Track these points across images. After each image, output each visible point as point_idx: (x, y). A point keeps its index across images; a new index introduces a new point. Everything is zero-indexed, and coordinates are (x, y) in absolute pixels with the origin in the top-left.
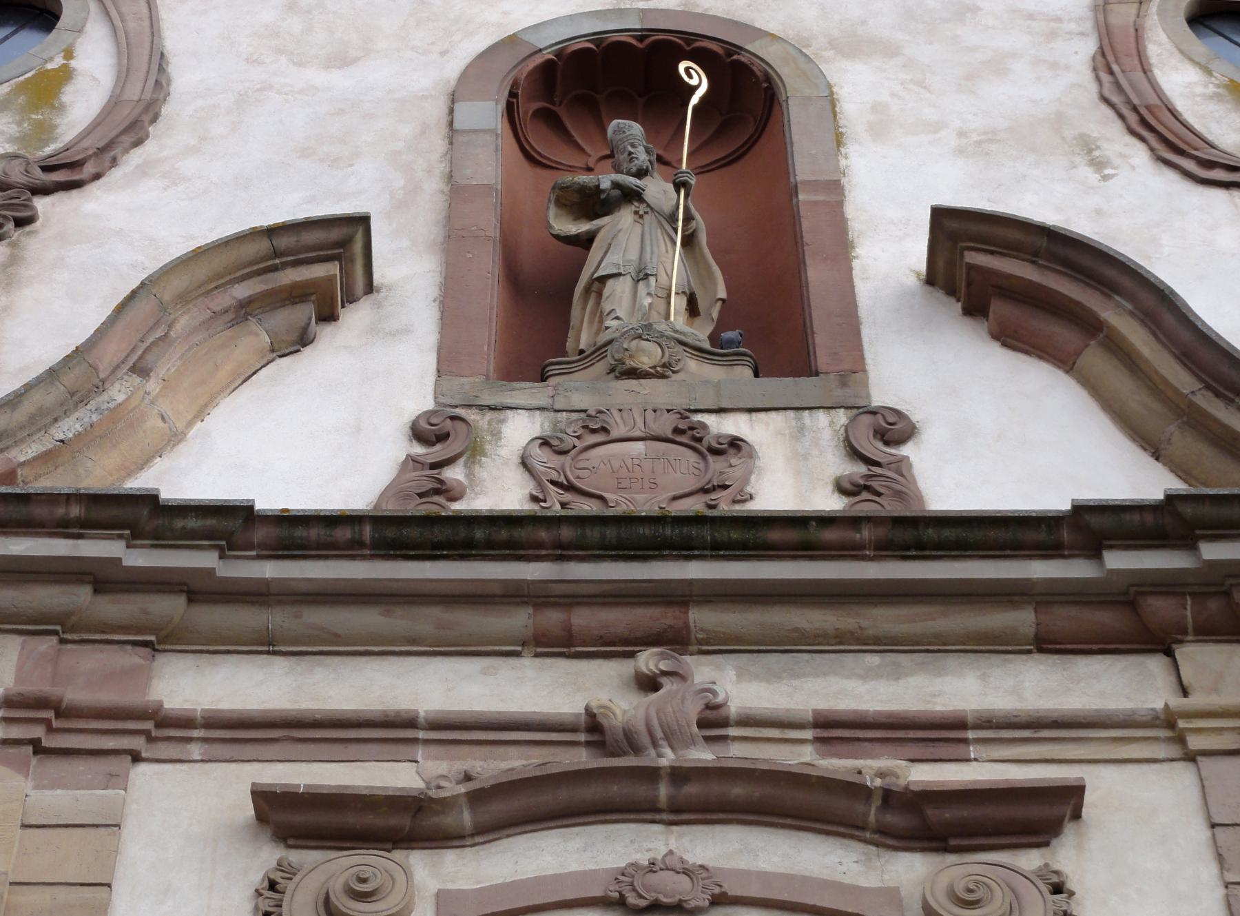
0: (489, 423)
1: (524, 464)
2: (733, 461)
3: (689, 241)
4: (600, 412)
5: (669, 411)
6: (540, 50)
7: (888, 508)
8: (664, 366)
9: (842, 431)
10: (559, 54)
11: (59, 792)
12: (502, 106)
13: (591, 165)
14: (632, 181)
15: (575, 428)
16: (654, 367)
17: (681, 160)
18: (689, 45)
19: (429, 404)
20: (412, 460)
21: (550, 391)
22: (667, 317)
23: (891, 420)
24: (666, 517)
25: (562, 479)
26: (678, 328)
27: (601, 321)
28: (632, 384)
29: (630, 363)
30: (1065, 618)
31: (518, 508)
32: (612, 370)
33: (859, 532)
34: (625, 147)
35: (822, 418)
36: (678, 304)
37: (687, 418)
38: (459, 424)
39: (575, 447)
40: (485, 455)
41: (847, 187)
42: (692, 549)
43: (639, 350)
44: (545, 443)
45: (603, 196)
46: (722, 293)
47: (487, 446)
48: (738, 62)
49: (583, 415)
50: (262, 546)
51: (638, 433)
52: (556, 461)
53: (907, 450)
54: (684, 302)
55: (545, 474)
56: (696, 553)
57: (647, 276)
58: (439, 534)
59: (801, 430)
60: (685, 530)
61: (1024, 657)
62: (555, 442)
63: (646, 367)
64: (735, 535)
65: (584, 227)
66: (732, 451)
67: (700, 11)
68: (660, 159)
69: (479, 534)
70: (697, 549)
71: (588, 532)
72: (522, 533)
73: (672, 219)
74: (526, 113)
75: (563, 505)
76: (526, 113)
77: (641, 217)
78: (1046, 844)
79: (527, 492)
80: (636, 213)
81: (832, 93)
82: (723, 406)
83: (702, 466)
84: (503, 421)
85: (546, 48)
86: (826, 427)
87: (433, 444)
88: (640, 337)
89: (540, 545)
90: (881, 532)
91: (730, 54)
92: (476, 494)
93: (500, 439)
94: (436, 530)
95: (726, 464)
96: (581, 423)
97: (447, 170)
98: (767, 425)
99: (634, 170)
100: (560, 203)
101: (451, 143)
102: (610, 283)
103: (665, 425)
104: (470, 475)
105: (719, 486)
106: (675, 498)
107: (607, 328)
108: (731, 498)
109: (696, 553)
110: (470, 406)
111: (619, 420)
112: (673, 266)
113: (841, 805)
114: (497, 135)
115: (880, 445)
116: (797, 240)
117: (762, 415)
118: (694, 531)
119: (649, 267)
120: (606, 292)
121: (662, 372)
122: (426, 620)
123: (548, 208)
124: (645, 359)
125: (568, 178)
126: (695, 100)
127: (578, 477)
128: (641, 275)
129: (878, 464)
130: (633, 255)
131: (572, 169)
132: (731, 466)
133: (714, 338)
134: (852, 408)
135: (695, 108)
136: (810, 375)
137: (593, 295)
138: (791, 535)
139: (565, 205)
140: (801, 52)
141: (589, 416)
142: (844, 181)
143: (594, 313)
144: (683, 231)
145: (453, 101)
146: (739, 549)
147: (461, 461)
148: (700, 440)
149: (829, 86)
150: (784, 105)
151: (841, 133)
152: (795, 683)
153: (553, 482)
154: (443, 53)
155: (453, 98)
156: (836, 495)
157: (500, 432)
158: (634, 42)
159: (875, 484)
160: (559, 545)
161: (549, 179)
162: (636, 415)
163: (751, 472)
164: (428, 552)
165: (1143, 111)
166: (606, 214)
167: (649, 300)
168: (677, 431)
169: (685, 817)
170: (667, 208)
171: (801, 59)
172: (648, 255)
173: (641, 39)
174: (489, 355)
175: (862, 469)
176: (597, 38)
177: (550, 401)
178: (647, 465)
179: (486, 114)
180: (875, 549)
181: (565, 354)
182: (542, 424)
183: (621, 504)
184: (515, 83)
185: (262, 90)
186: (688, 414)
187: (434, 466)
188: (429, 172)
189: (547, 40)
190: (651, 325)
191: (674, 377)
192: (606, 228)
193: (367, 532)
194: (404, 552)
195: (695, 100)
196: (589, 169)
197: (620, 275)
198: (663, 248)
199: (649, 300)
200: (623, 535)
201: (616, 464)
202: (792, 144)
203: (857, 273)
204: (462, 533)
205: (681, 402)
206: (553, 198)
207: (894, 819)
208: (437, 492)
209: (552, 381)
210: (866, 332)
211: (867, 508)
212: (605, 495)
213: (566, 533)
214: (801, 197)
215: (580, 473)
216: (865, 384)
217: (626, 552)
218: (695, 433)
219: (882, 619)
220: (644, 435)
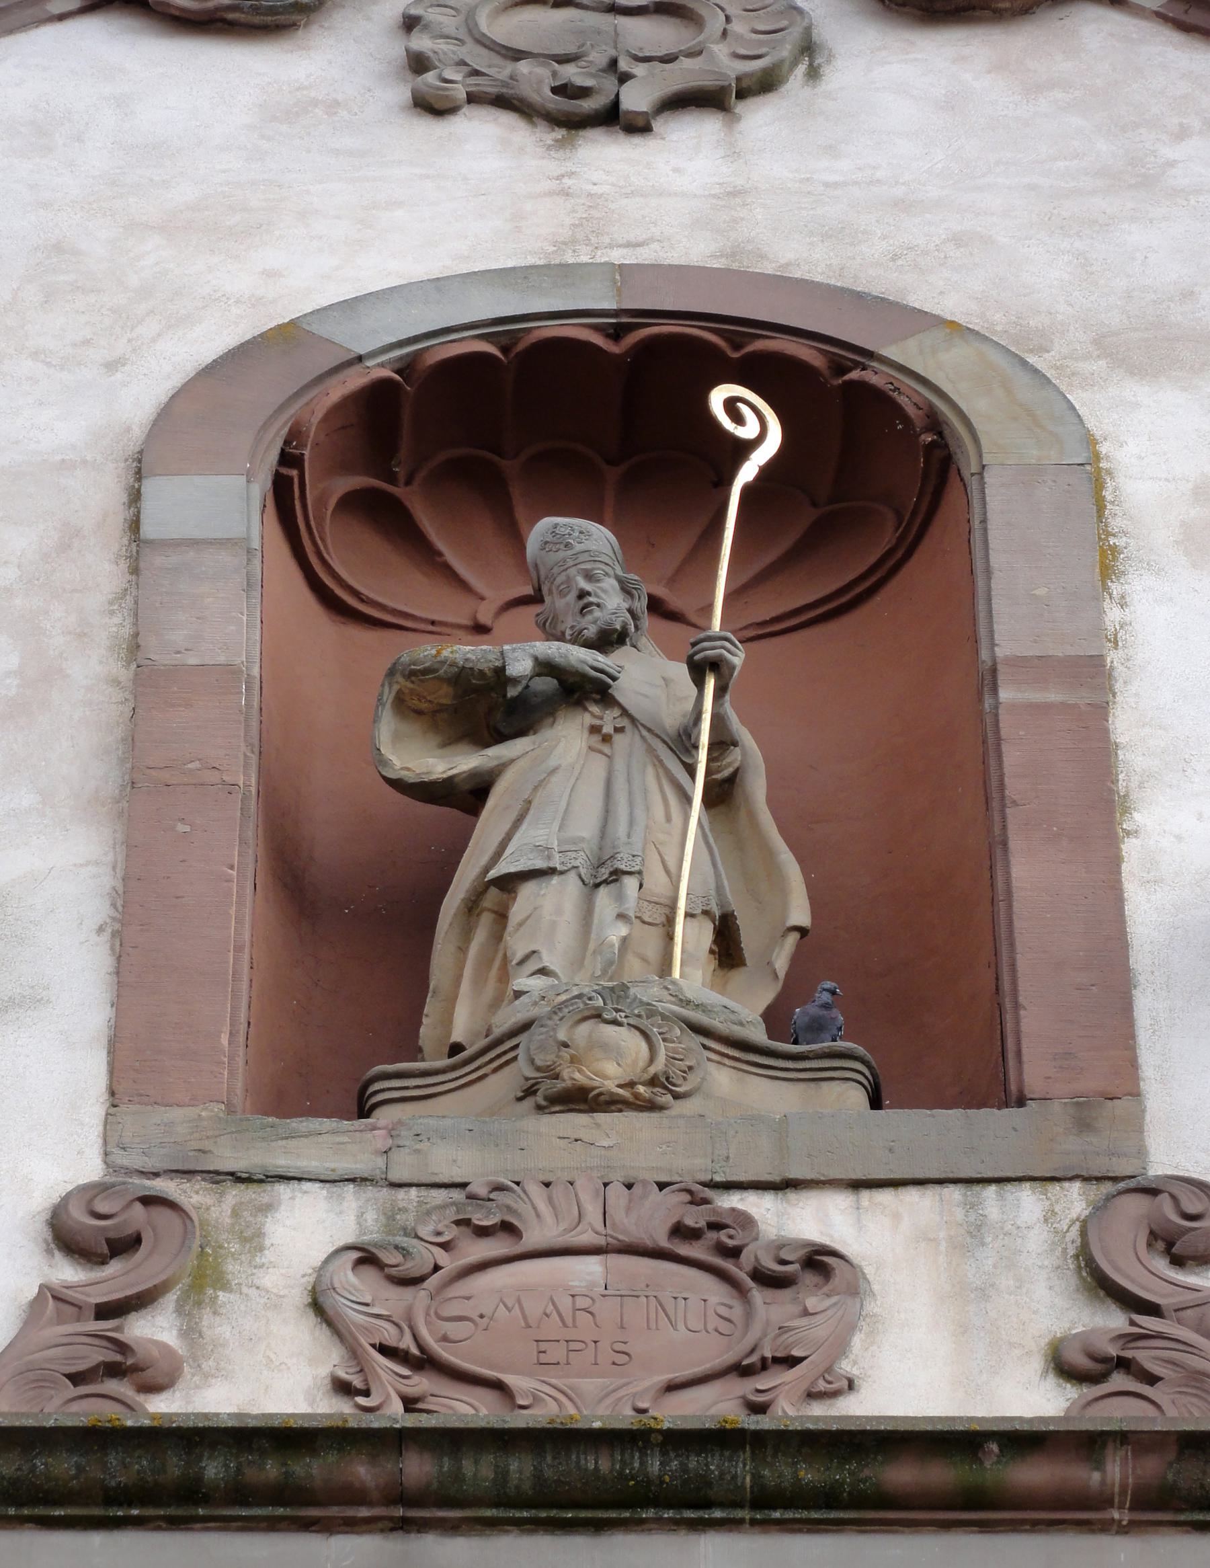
0: (235, 1213)
1: (318, 1307)
2: (812, 1303)
3: (722, 794)
4: (499, 1188)
5: (662, 1186)
6: (360, 359)
7: (1171, 1412)
8: (653, 1082)
9: (1075, 1231)
10: (407, 368)
12: (262, 485)
13: (485, 618)
14: (579, 657)
15: (438, 1225)
16: (631, 1085)
17: (710, 607)
18: (737, 347)
19: (91, 1169)
20: (54, 1298)
21: (380, 1140)
22: (665, 968)
23: (1192, 1208)
24: (651, 1431)
25: (407, 1343)
26: (689, 995)
27: (504, 976)
28: (577, 1123)
29: (573, 1076)
31: (303, 1408)
32: (530, 1092)
33: (1099, 1466)
34: (569, 580)
36: (691, 937)
37: (706, 1201)
38: (161, 1215)
39: (437, 1268)
40: (225, 1286)
41: (1120, 671)
42: (708, 1505)
43: (595, 1045)
44: (367, 1258)
45: (512, 692)
46: (800, 915)
47: (231, 1267)
48: (862, 385)
49: (457, 1195)
51: (586, 1237)
52: (393, 1300)
54: (705, 934)
55: (366, 1330)
56: (718, 1514)
57: (617, 875)
58: (120, 1469)
59: (976, 1231)
60: (693, 1462)
62: (389, 1258)
63: (611, 1086)
64: (808, 1474)
65: (463, 762)
66: (809, 1278)
67: (769, 268)
68: (656, 606)
69: (213, 1469)
70: (722, 1505)
71: (468, 1467)
72: (313, 1469)
73: (684, 743)
74: (321, 501)
75: (410, 1404)
76: (321, 501)
77: (607, 739)
79: (324, 1371)
80: (595, 730)
81: (1097, 457)
82: (795, 1173)
83: (737, 1312)
84: (267, 1208)
85: (373, 354)
86: (1034, 1223)
87: (103, 1261)
88: (598, 1016)
89: (355, 1496)
90: (1151, 1468)
91: (840, 368)
92: (206, 1376)
93: (261, 1249)
94: (113, 1460)
95: (797, 1309)
96: (451, 1214)
97: (127, 631)
98: (896, 1217)
99: (591, 632)
100: (402, 705)
101: (135, 570)
102: (527, 891)
103: (653, 1218)
104: (190, 1333)
105: (776, 1360)
106: (672, 1387)
107: (518, 994)
108: (804, 1386)
109: (718, 1514)
110: (188, 1173)
111: (543, 1207)
112: (683, 852)
114: (249, 551)
115: (1161, 1265)
116: (989, 794)
117: (885, 1197)
118: (714, 1464)
119: (622, 855)
120: (518, 911)
121: (649, 1096)
123: (376, 720)
124: (611, 1068)
125: (425, 651)
126: (748, 472)
127: (445, 1339)
128: (604, 873)
129: (1153, 1310)
130: (585, 827)
131: (435, 628)
132: (806, 1313)
133: (774, 1018)
134: (1099, 1179)
135: (747, 490)
136: (1007, 1105)
137: (486, 920)
138: (939, 1474)
139: (419, 713)
140: (1024, 363)
141: (471, 1197)
142: (1113, 658)
143: (485, 964)
144: (708, 772)
145: (139, 475)
146: (818, 1507)
147: (170, 1300)
148: (734, 1253)
149: (1090, 441)
150: (973, 484)
151: (1114, 549)
153: (385, 1350)
154: (112, 366)
155: (139, 470)
156: (1052, 1380)
157: (260, 1234)
158: (597, 339)
159: (1144, 1356)
160: (399, 1495)
161: (377, 651)
162: (585, 1197)
163: (852, 1328)
164: (96, 1511)
166: (521, 733)
167: (623, 930)
168: (680, 1231)
170: (671, 718)
171: (1022, 379)
172: (621, 829)
173: (616, 332)
174: (231, 1058)
175: (1116, 1320)
176: (504, 330)
177: (380, 1162)
178: (607, 1310)
179: (223, 503)
180: (1137, 1506)
181: (416, 1052)
182: (360, 1215)
183: (544, 1402)
184: (295, 435)
186: (708, 1193)
187: (106, 1311)
188: (82, 635)
189: (377, 337)
190: (624, 988)
191: (679, 1107)
192: (521, 763)
194: (40, 1511)
195: (748, 472)
196: (480, 629)
197: (551, 872)
198: (658, 811)
199: (623, 930)
200: (548, 1473)
201: (534, 1308)
202: (988, 572)
203: (1131, 869)
204: (174, 1466)
205: (694, 1165)
206: (389, 697)
208: (113, 1370)
209: (384, 1116)
210: (1147, 1006)
211: (1120, 1412)
212: (509, 1379)
213: (417, 1468)
214: (1005, 694)
215: (451, 1328)
216: (1136, 1124)
217: (553, 1513)
218: (723, 1236)
220: (601, 1241)
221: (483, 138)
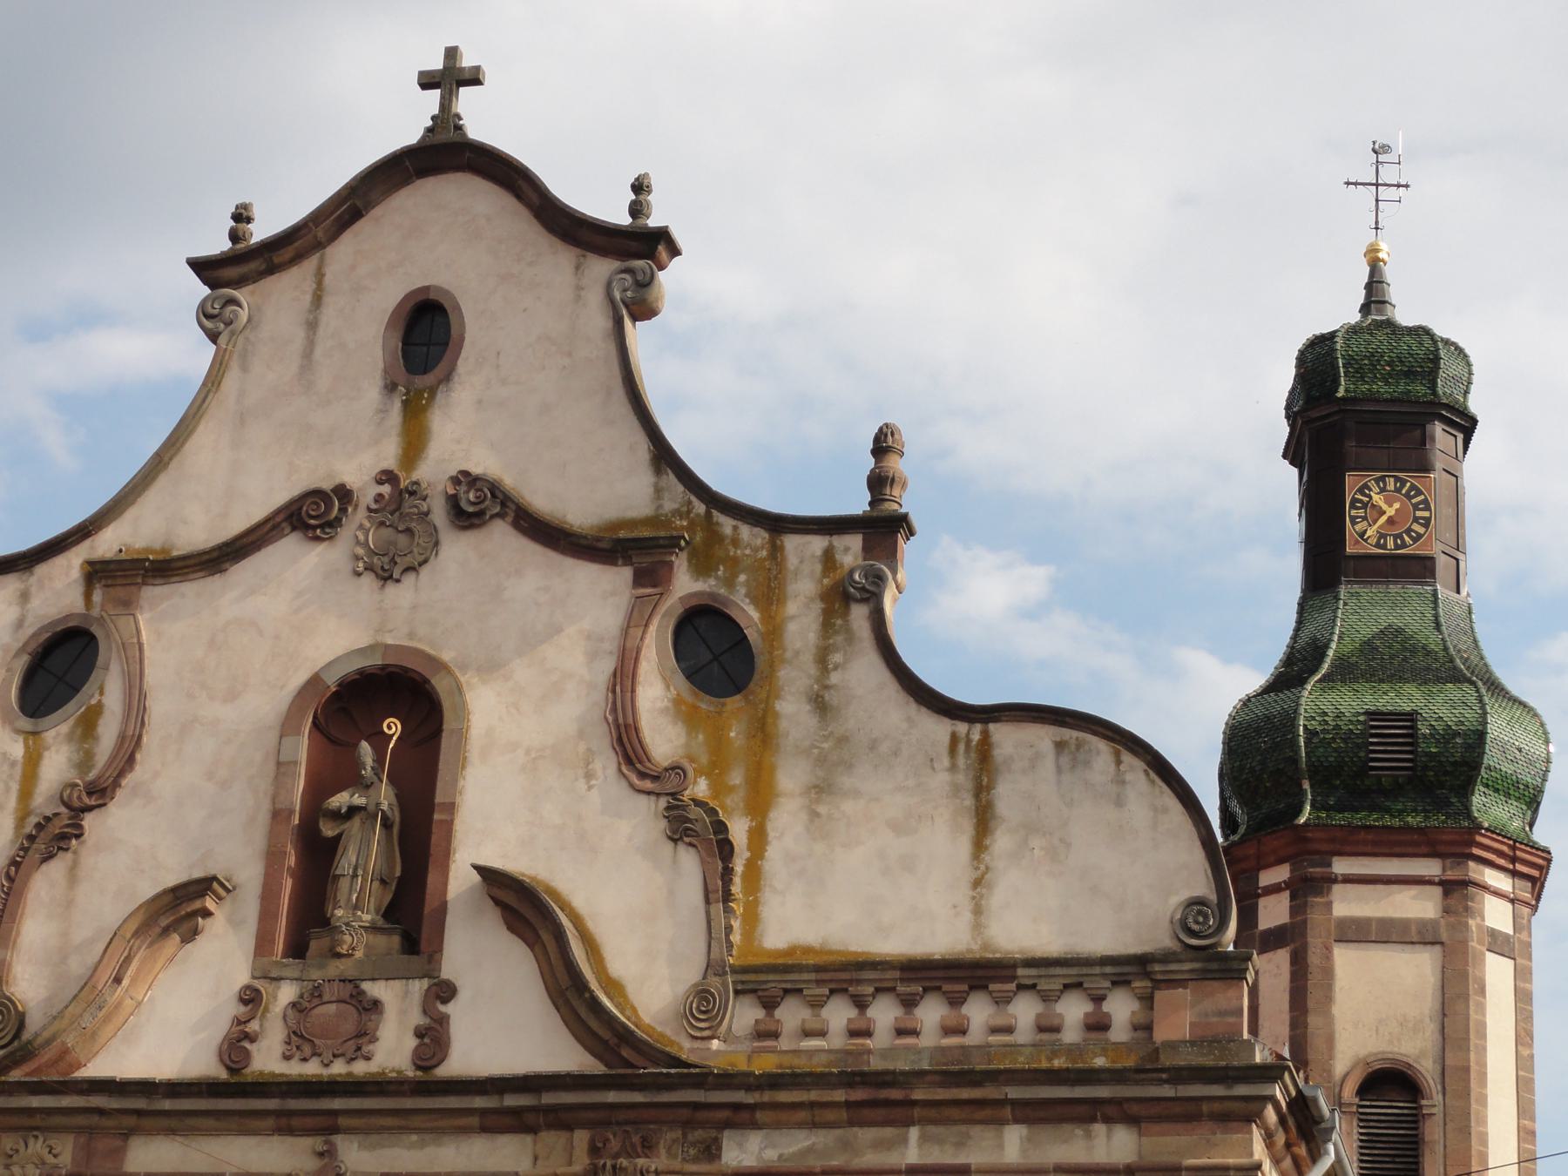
35: (417, 982)
86: (418, 987)
165: (623, 729)
193: (320, 234)
214: (436, 816)
219: (416, 1121)
221: (368, 580)
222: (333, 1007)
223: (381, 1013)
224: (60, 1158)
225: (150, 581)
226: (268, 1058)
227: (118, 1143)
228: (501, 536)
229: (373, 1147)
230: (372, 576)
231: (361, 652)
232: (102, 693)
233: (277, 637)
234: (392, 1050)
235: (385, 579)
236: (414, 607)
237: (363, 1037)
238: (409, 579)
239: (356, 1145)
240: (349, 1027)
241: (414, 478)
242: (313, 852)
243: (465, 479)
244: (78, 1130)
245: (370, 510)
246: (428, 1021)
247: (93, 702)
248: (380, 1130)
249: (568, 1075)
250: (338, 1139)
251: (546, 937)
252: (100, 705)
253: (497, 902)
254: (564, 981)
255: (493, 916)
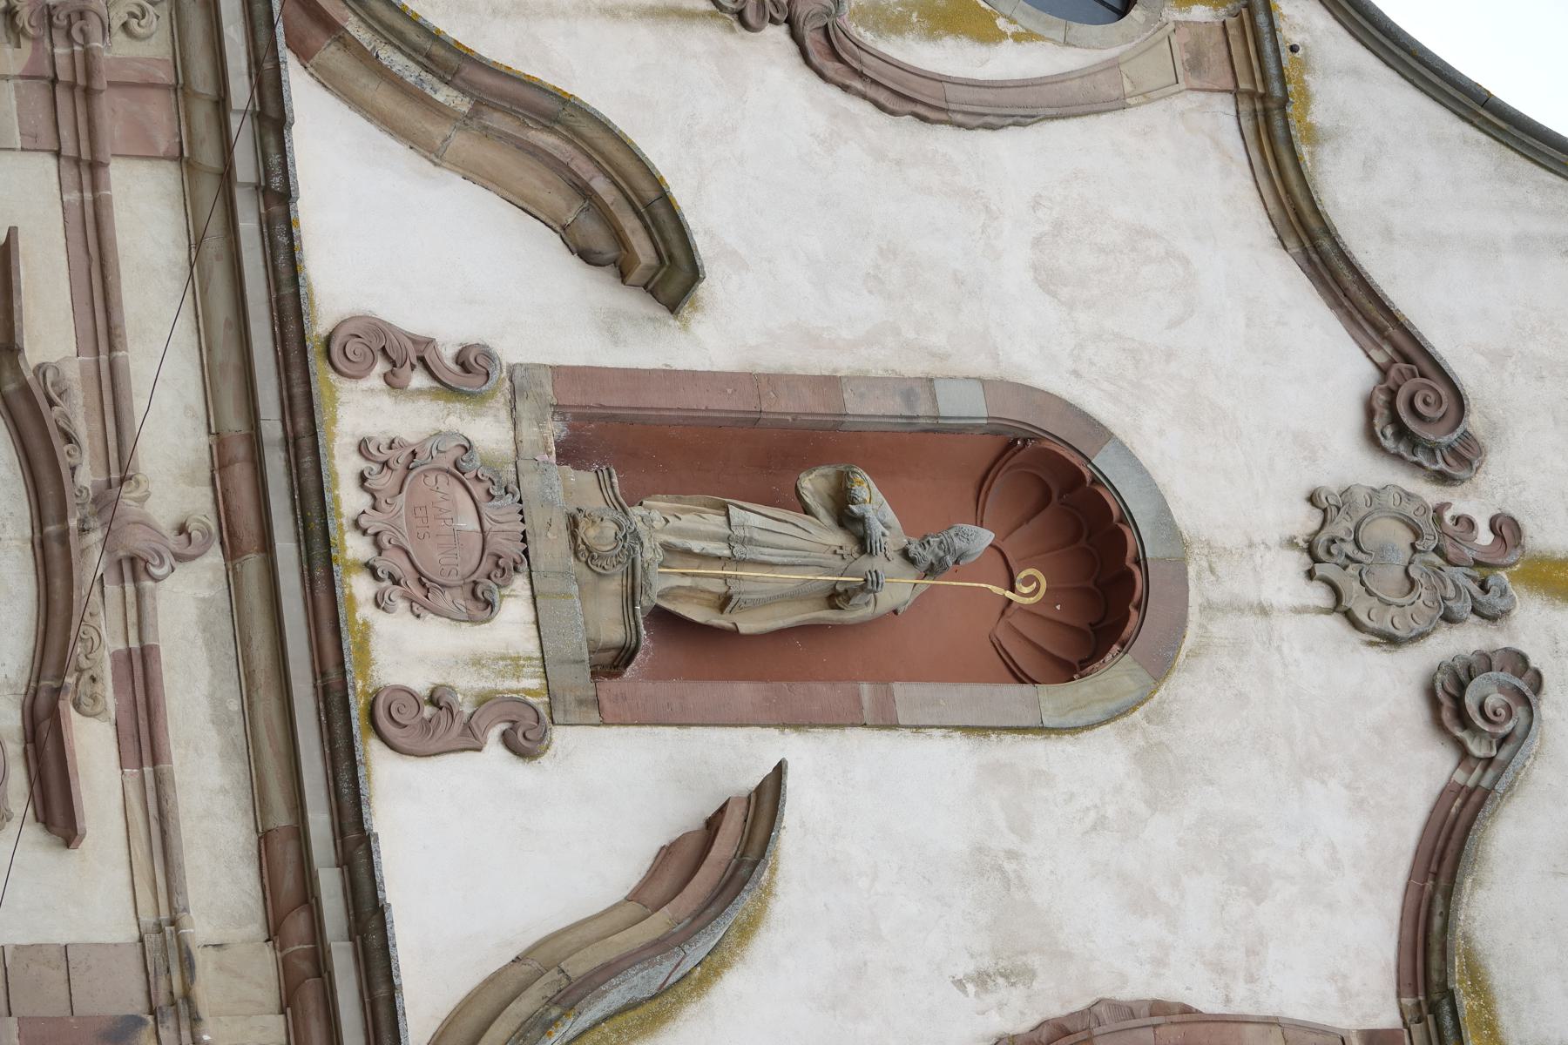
11: (14, 103)
30: (286, 854)
50: (268, 215)
51: (487, 525)
53: (494, 749)
61: (252, 826)
71: (308, 459)
78: (37, 820)
113: (52, 658)
122: (227, 355)
152: (200, 642)
169: (38, 550)
185: (987, 209)
189: (1105, 462)
207: (43, 697)
214: (865, 689)
219: (267, 704)
221: (1304, 521)
222: (469, 523)
223: (472, 620)
224: (119, 37)
225: (1245, 107)
226: (359, 413)
227: (164, 143)
228: (1427, 768)
229: (206, 627)
230: (1314, 524)
231: (1164, 511)
232: (1017, 38)
233: (1170, 355)
234: (406, 649)
235: (1310, 550)
236: (1264, 611)
237: (422, 591)
238: (1318, 595)
239: (206, 593)
240: (433, 559)
241: (1512, 591)
242: (763, 446)
243: (1526, 682)
244: (180, 60)
245: (1439, 510)
246: (467, 710)
247: (1001, 23)
248: (241, 638)
249: (393, 989)
250: (214, 557)
251: (658, 924)
252: (996, 37)
253: (713, 825)
254: (579, 966)
255: (686, 815)
